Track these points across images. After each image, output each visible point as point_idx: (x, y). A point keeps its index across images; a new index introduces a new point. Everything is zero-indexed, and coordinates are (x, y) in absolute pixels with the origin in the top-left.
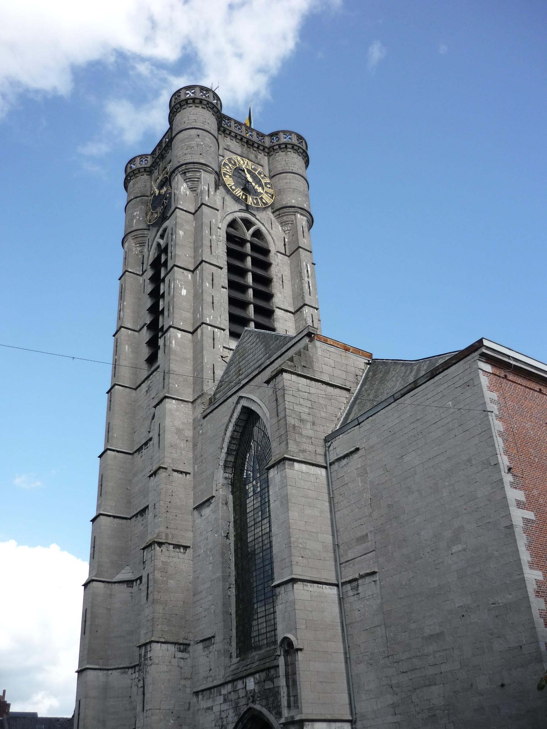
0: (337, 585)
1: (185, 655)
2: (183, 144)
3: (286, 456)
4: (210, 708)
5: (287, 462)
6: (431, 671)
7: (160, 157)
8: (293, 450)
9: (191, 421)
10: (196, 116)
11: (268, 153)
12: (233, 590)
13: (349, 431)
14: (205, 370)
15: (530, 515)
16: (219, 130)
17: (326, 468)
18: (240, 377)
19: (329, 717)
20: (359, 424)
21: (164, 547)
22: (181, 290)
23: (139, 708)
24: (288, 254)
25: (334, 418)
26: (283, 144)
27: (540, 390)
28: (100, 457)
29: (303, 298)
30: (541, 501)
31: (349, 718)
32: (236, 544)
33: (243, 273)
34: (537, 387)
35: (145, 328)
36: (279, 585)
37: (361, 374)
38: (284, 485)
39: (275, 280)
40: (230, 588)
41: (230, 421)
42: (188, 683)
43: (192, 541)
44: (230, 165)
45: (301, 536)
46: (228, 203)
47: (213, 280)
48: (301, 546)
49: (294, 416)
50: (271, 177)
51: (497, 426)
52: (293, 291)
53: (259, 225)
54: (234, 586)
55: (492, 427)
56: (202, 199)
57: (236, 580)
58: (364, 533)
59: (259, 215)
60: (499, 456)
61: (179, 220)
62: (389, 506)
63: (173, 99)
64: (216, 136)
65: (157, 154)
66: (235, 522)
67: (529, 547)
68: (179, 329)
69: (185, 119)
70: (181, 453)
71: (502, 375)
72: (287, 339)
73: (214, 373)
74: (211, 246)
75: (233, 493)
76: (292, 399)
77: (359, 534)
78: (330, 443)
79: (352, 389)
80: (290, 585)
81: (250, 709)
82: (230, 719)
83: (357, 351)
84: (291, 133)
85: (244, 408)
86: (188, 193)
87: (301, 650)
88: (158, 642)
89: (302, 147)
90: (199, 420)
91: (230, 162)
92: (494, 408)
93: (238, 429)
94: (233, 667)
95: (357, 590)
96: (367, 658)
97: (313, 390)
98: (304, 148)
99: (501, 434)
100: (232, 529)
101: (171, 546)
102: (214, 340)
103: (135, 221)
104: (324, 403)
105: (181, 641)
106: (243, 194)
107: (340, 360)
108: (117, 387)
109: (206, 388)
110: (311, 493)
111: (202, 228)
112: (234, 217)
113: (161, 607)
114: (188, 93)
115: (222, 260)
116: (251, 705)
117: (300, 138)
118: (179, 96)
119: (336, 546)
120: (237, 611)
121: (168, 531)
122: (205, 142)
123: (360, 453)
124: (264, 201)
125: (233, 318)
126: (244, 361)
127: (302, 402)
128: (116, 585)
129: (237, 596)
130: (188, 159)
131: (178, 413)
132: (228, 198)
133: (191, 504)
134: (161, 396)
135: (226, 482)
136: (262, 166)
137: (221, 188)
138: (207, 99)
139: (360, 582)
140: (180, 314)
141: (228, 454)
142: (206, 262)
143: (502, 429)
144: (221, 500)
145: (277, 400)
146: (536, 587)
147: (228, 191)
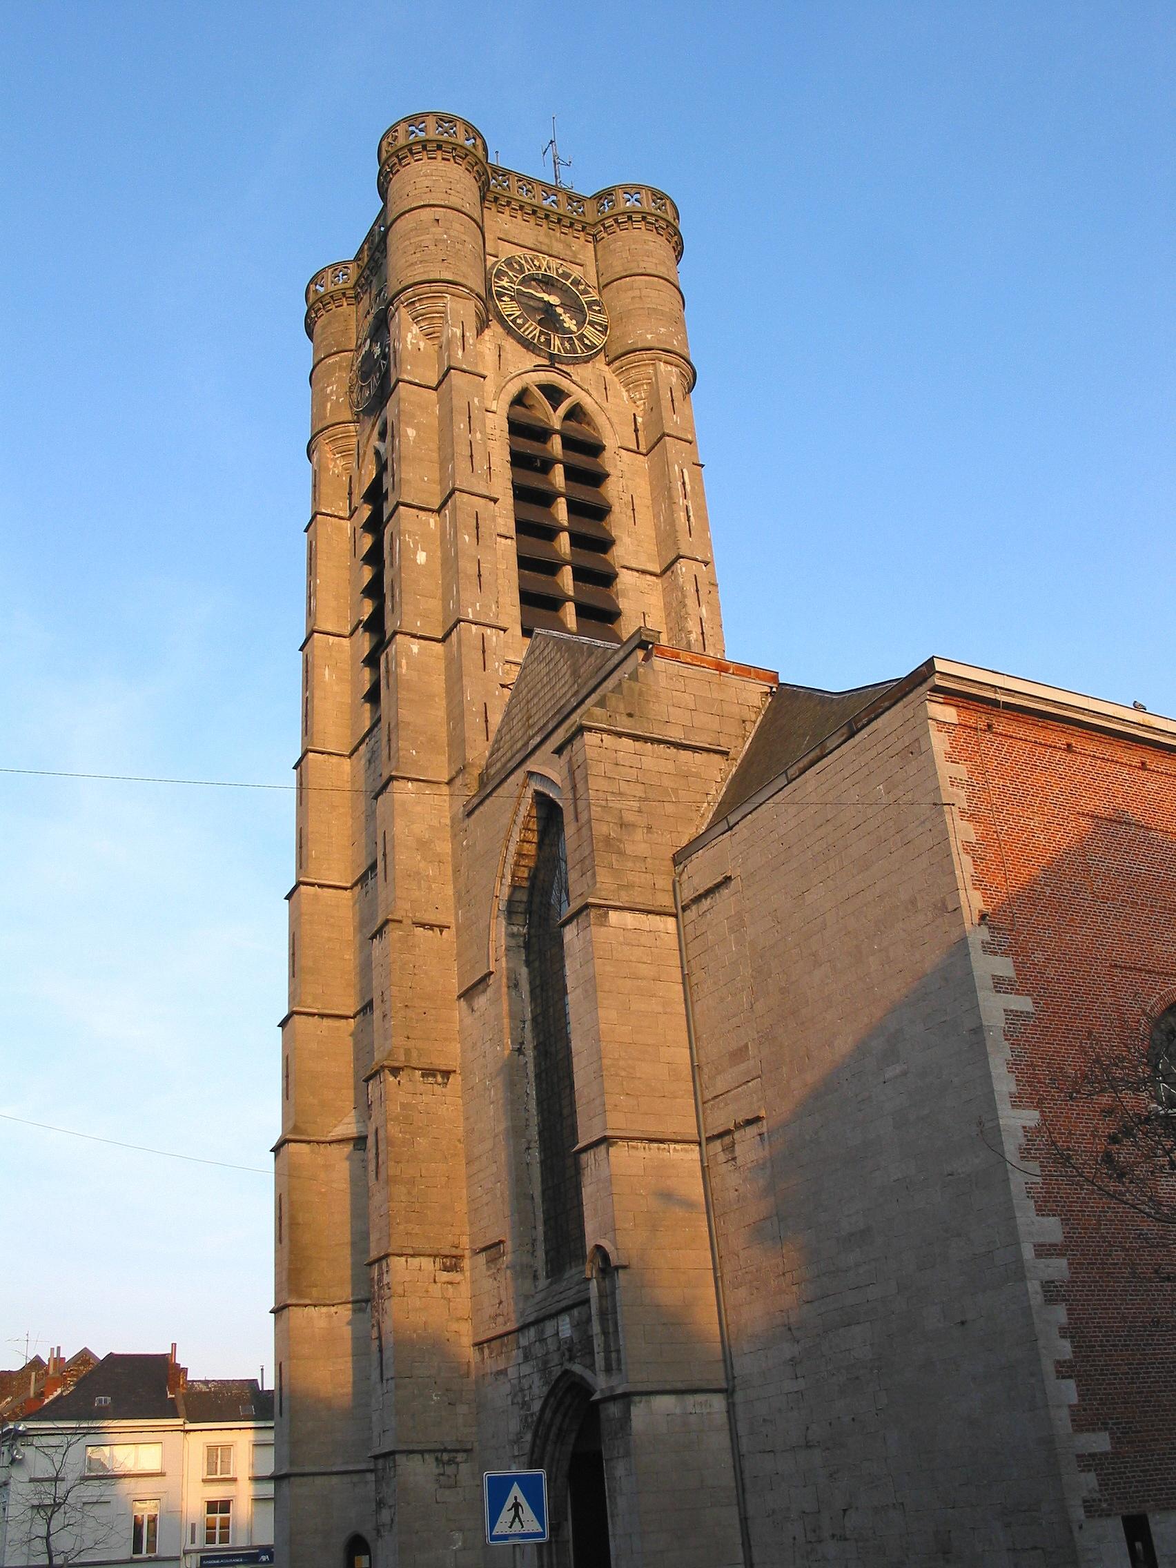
2: (407, 243)
3: (591, 900)
4: (503, 1372)
9: (448, 822)
12: (536, 1153)
13: (714, 842)
14: (468, 718)
15: (1023, 1004)
16: (483, 199)
17: (676, 916)
19: (680, 1386)
20: (730, 828)
22: (415, 554)
23: (375, 1375)
24: (643, 449)
25: (694, 815)
26: (623, 213)
27: (1069, 745)
28: (288, 897)
29: (676, 542)
30: (1050, 973)
31: (724, 1385)
32: (537, 1065)
33: (546, 499)
34: (1062, 742)
35: (361, 630)
37: (753, 717)
38: (589, 958)
39: (616, 509)
40: (528, 1148)
43: (459, 1060)
45: (623, 1054)
46: (509, 356)
47: (477, 528)
48: (623, 1074)
51: (962, 831)
52: (657, 528)
53: (578, 395)
55: (951, 834)
57: (540, 1133)
59: (580, 372)
60: (961, 892)
61: (405, 406)
62: (783, 991)
63: (384, 143)
64: (476, 216)
65: (366, 260)
66: (534, 1019)
67: (1013, 1066)
68: (414, 636)
69: (408, 188)
70: (430, 888)
71: (982, 726)
73: (487, 721)
75: (528, 963)
76: (603, 784)
78: (681, 866)
79: (732, 752)
80: (603, 1147)
81: (566, 1372)
82: (536, 1391)
83: (745, 671)
84: (639, 188)
86: (422, 345)
87: (625, 1267)
88: (401, 1255)
89: (664, 216)
91: (513, 269)
92: (960, 797)
93: (530, 836)
94: (539, 1297)
95: (733, 1151)
96: (749, 1277)
97: (648, 762)
99: (968, 848)
100: (528, 1035)
103: (329, 405)
104: (672, 785)
108: (310, 755)
109: (471, 755)
110: (644, 970)
111: (452, 419)
112: (524, 385)
113: (404, 1190)
114: (413, 132)
115: (502, 482)
116: (568, 1366)
117: (659, 196)
119: (696, 1069)
120: (543, 1192)
122: (453, 233)
124: (587, 342)
125: (528, 598)
126: (536, 700)
127: (624, 787)
128: (334, 1146)
129: (542, 1162)
130: (418, 274)
131: (419, 808)
132: (510, 345)
133: (455, 985)
134: (385, 776)
135: (513, 942)
138: (451, 139)
139: (737, 1135)
140: (417, 607)
141: (514, 888)
143: (973, 839)
144: (504, 980)
146: (1023, 1141)
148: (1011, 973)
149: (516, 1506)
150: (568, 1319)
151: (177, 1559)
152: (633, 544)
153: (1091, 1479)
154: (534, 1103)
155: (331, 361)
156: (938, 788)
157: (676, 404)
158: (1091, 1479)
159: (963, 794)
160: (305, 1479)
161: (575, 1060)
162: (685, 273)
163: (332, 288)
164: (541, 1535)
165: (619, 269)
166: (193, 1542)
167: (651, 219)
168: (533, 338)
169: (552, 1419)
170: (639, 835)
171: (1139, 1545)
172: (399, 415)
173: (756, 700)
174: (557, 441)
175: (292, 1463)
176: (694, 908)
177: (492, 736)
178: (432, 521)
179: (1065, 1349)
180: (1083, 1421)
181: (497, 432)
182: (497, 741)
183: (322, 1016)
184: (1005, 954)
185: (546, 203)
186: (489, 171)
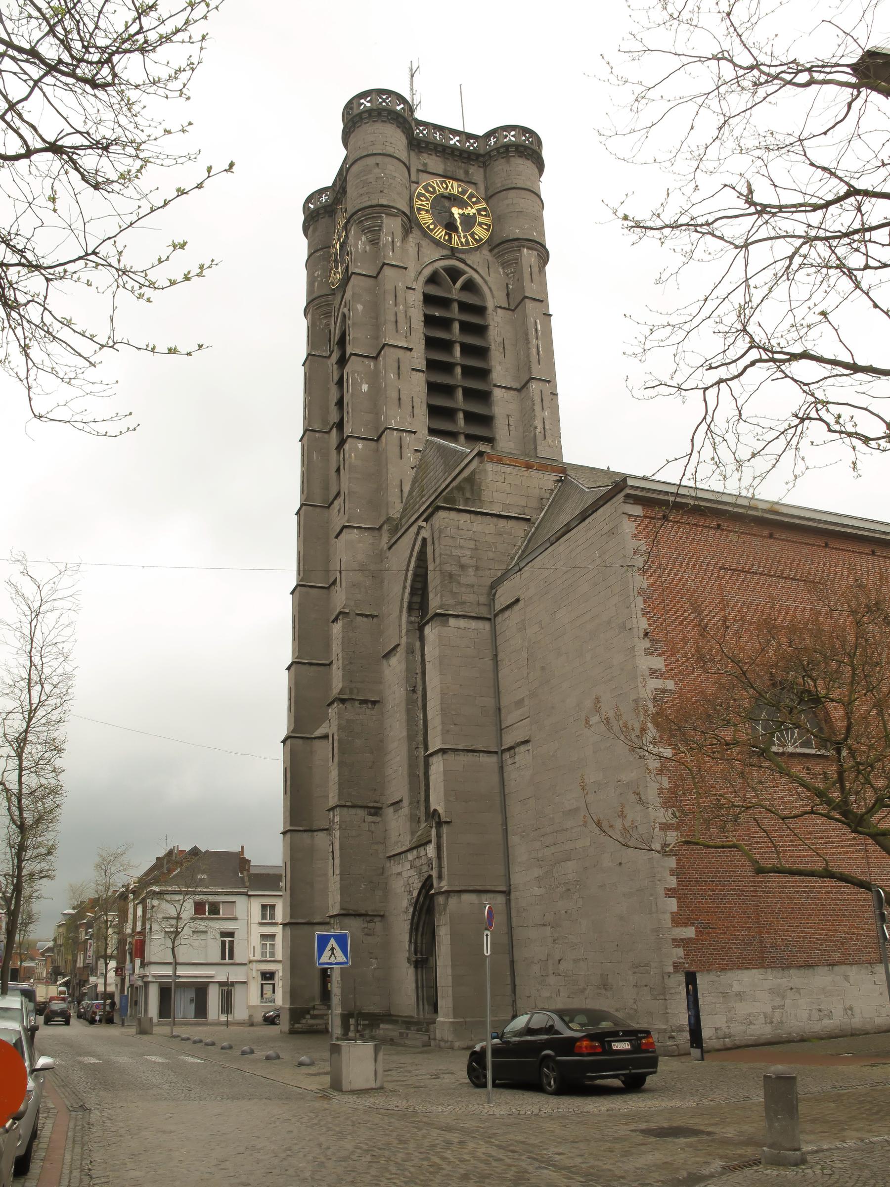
1: (378, 819)
4: (400, 874)
11: (484, 163)
20: (520, 570)
21: (348, 705)
29: (530, 368)
31: (503, 888)
37: (548, 496)
39: (493, 347)
41: (411, 555)
44: (427, 195)
48: (453, 712)
50: (487, 199)
55: (631, 584)
64: (404, 157)
71: (659, 516)
74: (396, 322)
101: (357, 703)
105: (372, 804)
118: (352, 109)
122: (387, 172)
123: (521, 603)
124: (477, 237)
125: (434, 411)
127: (462, 542)
132: (425, 243)
136: (475, 184)
137: (416, 231)
139: (517, 750)
141: (412, 594)
143: (645, 586)
148: (663, 667)
149: (333, 949)
151: (245, 964)
153: (680, 952)
157: (534, 276)
158: (680, 952)
164: (347, 963)
166: (254, 956)
168: (440, 238)
170: (471, 572)
171: (690, 987)
173: (551, 486)
178: (372, 364)
179: (673, 882)
180: (678, 920)
181: (416, 303)
182: (406, 504)
184: (659, 655)
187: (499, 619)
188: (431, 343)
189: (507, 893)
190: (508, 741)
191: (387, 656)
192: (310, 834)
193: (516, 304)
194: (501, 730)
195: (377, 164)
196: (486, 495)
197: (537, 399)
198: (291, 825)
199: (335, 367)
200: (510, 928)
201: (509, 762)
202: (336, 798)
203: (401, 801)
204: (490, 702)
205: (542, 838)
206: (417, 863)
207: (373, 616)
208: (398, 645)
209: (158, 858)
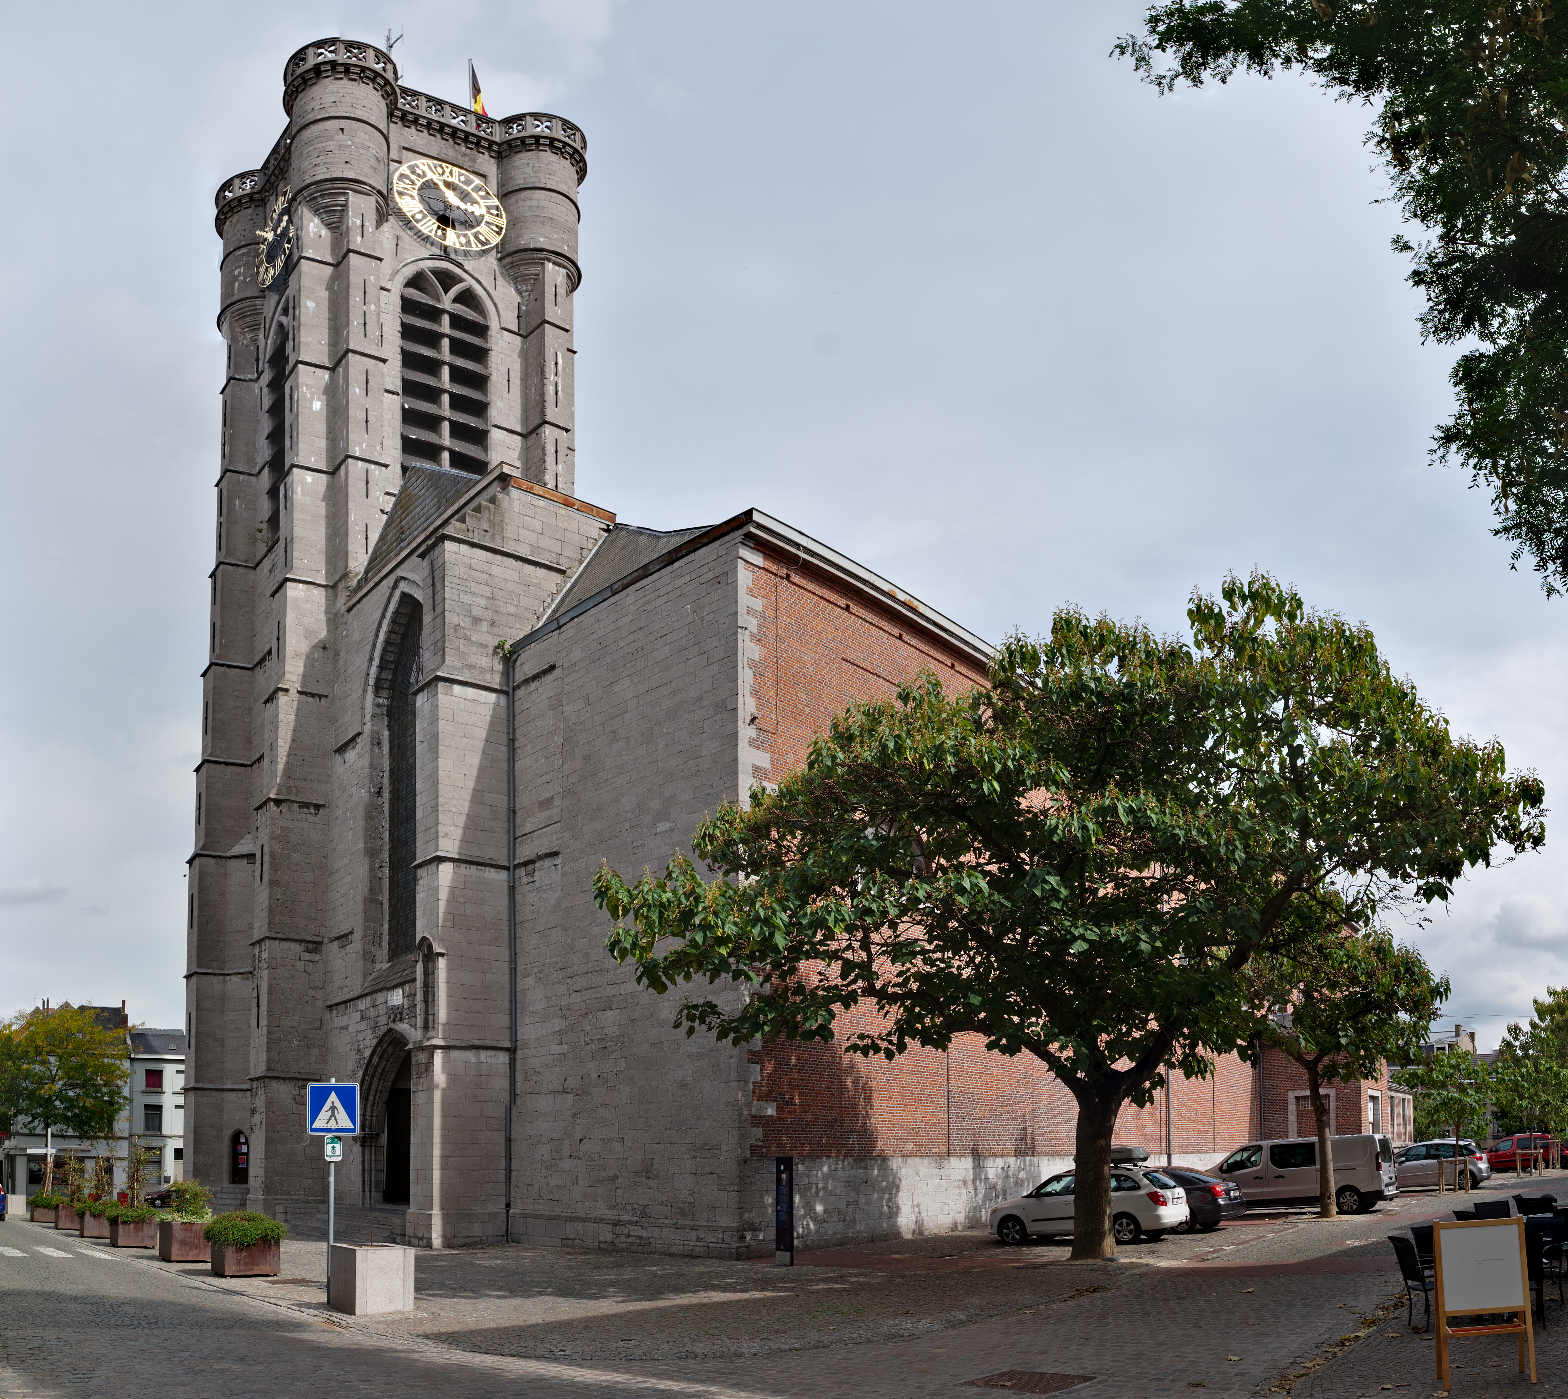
0: (507, 868)
1: (317, 957)
3: (439, 674)
4: (346, 1028)
5: (441, 685)
6: (608, 991)
7: (277, 172)
8: (451, 667)
10: (333, 94)
12: (386, 871)
16: (390, 115)
17: (506, 693)
18: (402, 544)
20: (559, 628)
21: (284, 807)
22: (311, 403)
25: (531, 616)
29: (543, 408)
36: (421, 865)
37: (590, 546)
38: (434, 720)
41: (383, 616)
42: (319, 994)
46: (406, 246)
48: (454, 810)
49: (458, 610)
54: (387, 865)
56: (348, 242)
58: (549, 795)
60: (740, 697)
62: (587, 758)
64: (383, 127)
65: (272, 168)
72: (471, 483)
74: (365, 324)
75: (389, 727)
77: (543, 796)
79: (569, 572)
80: (434, 865)
83: (588, 509)
85: (404, 595)
90: (343, 615)
92: (752, 624)
96: (536, 970)
97: (496, 571)
98: (577, 146)
99: (752, 664)
101: (296, 806)
102: (367, 483)
103: (237, 284)
106: (439, 227)
107: (553, 522)
114: (322, 54)
115: (392, 346)
116: (392, 1025)
117: (567, 125)
120: (390, 899)
121: (291, 783)
122: (355, 140)
123: (557, 673)
127: (475, 587)
128: (233, 860)
132: (406, 237)
135: (378, 711)
139: (537, 865)
141: (382, 667)
142: (549, 323)
143: (757, 658)
145: (433, 585)
147: (407, 223)
150: (401, 991)
152: (505, 406)
154: (387, 834)
155: (239, 252)
156: (736, 613)
159: (755, 622)
160: (205, 1092)
161: (418, 798)
162: (584, 194)
163: (240, 193)
165: (521, 181)
167: (557, 144)
169: (378, 1063)
170: (484, 626)
172: (299, 290)
174: (446, 319)
175: (196, 1081)
176: (523, 688)
177: (370, 550)
181: (391, 307)
183: (227, 764)
185: (454, 122)
186: (398, 91)
187: (520, 693)
188: (409, 360)
189: (512, 1051)
190: (525, 852)
191: (341, 750)
192: (221, 978)
193: (530, 329)
194: (515, 839)
195: (342, 130)
196: (510, 531)
197: (550, 449)
198: (198, 966)
199: (266, 390)
200: (513, 1094)
201: (525, 880)
202: (265, 928)
203: (351, 933)
204: (502, 801)
205: (569, 980)
206: (372, 1013)
207: (320, 696)
208: (360, 734)
209: (1188, 1076)
